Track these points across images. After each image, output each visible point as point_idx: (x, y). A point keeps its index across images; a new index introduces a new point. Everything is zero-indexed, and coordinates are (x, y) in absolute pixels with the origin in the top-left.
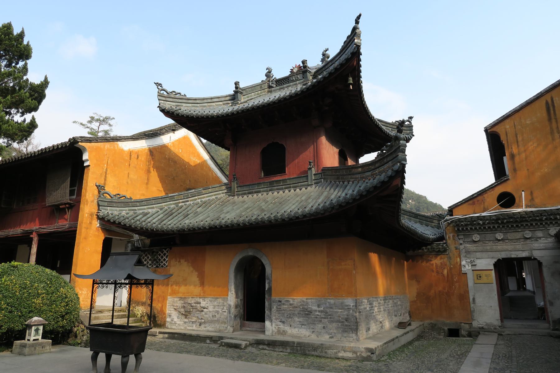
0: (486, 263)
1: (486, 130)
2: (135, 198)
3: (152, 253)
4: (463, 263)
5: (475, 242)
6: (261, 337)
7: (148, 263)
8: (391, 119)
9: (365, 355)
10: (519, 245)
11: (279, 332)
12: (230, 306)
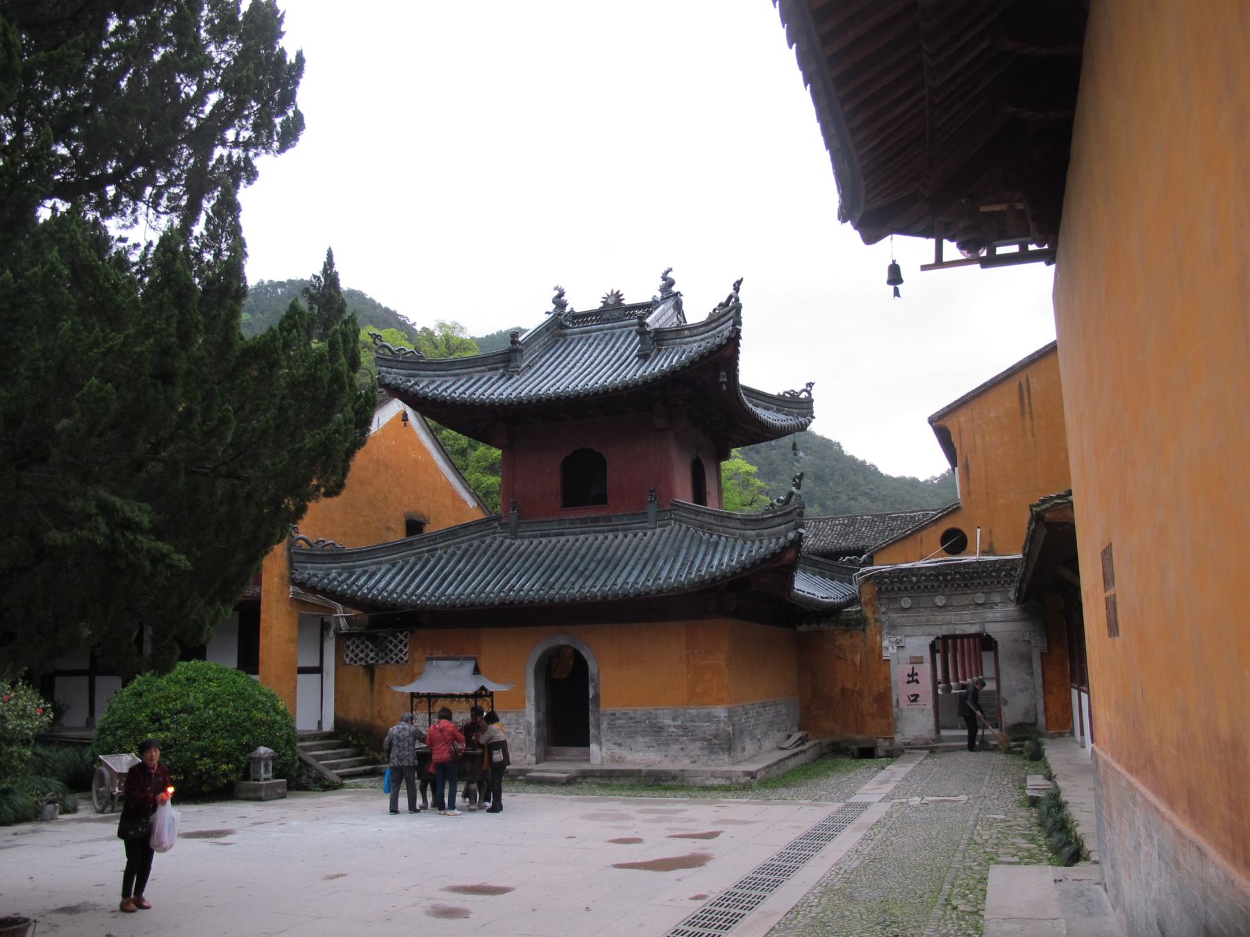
0: (919, 644)
1: (931, 421)
2: (348, 548)
3: (374, 639)
4: (885, 643)
5: (905, 610)
6: (586, 766)
7: (367, 655)
8: (773, 386)
9: (742, 780)
10: (967, 615)
11: (613, 759)
12: (529, 723)
